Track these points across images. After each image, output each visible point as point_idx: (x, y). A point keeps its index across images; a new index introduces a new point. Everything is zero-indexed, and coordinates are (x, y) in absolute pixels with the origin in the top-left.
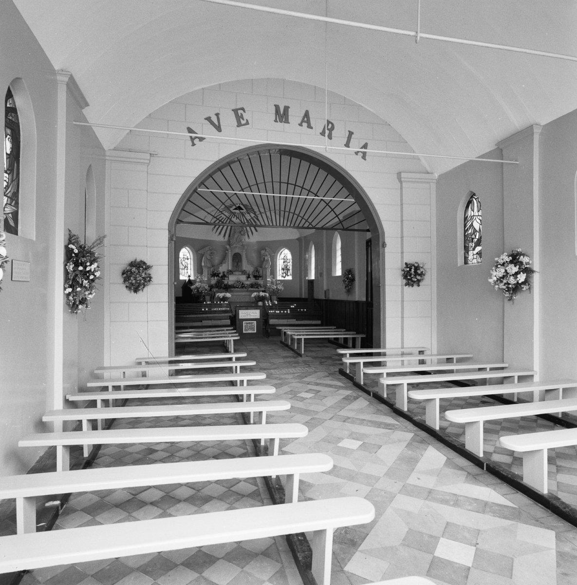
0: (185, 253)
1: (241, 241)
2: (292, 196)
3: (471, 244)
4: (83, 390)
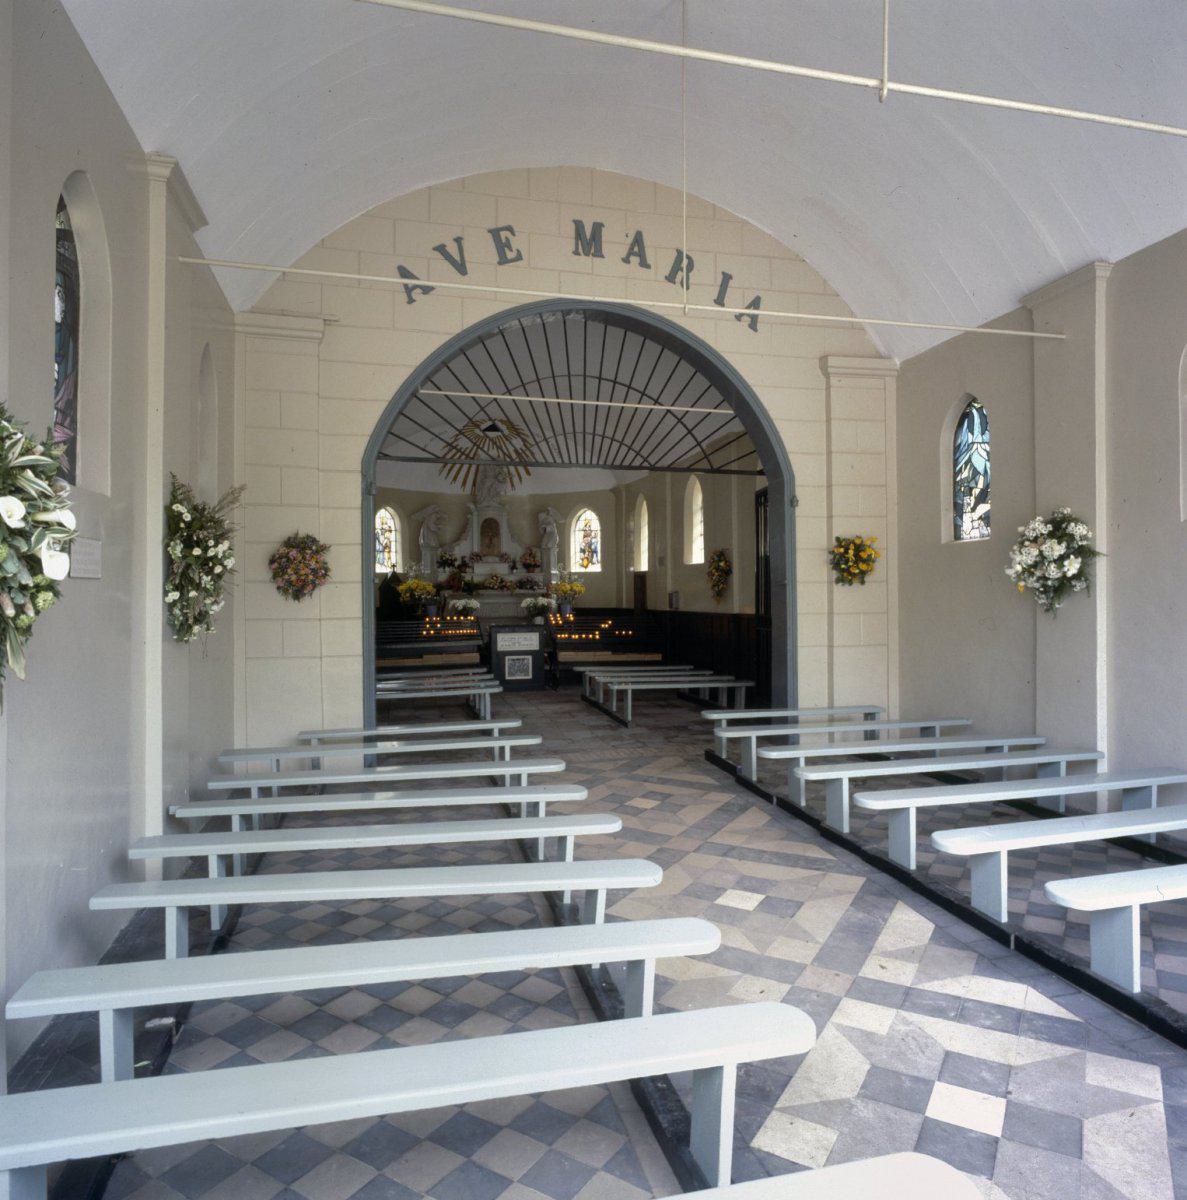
0: (385, 518)
1: (498, 494)
2: (622, 405)
3: (967, 500)
4: (198, 796)
